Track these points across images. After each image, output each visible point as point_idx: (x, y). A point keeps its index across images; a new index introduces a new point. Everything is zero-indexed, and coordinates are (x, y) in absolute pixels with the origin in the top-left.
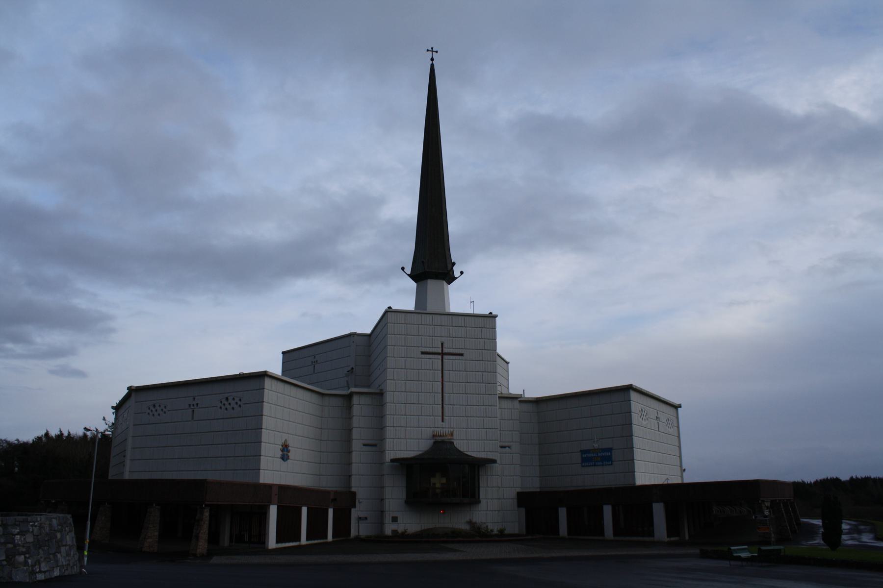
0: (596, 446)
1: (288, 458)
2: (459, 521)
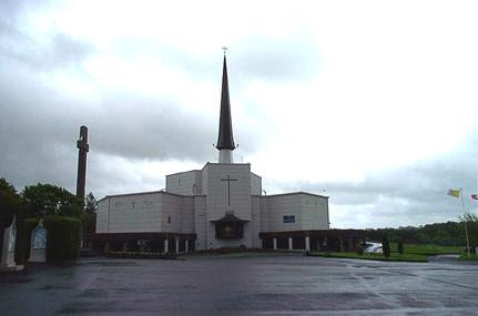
2: (237, 244)
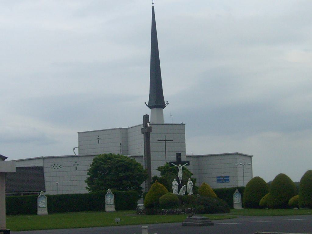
0: (223, 175)
1: (45, 191)
